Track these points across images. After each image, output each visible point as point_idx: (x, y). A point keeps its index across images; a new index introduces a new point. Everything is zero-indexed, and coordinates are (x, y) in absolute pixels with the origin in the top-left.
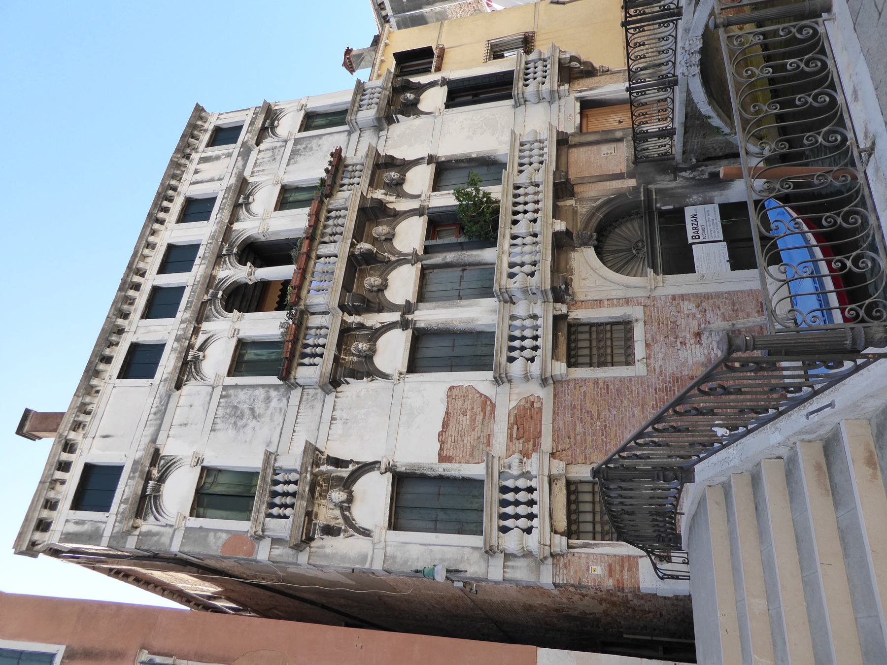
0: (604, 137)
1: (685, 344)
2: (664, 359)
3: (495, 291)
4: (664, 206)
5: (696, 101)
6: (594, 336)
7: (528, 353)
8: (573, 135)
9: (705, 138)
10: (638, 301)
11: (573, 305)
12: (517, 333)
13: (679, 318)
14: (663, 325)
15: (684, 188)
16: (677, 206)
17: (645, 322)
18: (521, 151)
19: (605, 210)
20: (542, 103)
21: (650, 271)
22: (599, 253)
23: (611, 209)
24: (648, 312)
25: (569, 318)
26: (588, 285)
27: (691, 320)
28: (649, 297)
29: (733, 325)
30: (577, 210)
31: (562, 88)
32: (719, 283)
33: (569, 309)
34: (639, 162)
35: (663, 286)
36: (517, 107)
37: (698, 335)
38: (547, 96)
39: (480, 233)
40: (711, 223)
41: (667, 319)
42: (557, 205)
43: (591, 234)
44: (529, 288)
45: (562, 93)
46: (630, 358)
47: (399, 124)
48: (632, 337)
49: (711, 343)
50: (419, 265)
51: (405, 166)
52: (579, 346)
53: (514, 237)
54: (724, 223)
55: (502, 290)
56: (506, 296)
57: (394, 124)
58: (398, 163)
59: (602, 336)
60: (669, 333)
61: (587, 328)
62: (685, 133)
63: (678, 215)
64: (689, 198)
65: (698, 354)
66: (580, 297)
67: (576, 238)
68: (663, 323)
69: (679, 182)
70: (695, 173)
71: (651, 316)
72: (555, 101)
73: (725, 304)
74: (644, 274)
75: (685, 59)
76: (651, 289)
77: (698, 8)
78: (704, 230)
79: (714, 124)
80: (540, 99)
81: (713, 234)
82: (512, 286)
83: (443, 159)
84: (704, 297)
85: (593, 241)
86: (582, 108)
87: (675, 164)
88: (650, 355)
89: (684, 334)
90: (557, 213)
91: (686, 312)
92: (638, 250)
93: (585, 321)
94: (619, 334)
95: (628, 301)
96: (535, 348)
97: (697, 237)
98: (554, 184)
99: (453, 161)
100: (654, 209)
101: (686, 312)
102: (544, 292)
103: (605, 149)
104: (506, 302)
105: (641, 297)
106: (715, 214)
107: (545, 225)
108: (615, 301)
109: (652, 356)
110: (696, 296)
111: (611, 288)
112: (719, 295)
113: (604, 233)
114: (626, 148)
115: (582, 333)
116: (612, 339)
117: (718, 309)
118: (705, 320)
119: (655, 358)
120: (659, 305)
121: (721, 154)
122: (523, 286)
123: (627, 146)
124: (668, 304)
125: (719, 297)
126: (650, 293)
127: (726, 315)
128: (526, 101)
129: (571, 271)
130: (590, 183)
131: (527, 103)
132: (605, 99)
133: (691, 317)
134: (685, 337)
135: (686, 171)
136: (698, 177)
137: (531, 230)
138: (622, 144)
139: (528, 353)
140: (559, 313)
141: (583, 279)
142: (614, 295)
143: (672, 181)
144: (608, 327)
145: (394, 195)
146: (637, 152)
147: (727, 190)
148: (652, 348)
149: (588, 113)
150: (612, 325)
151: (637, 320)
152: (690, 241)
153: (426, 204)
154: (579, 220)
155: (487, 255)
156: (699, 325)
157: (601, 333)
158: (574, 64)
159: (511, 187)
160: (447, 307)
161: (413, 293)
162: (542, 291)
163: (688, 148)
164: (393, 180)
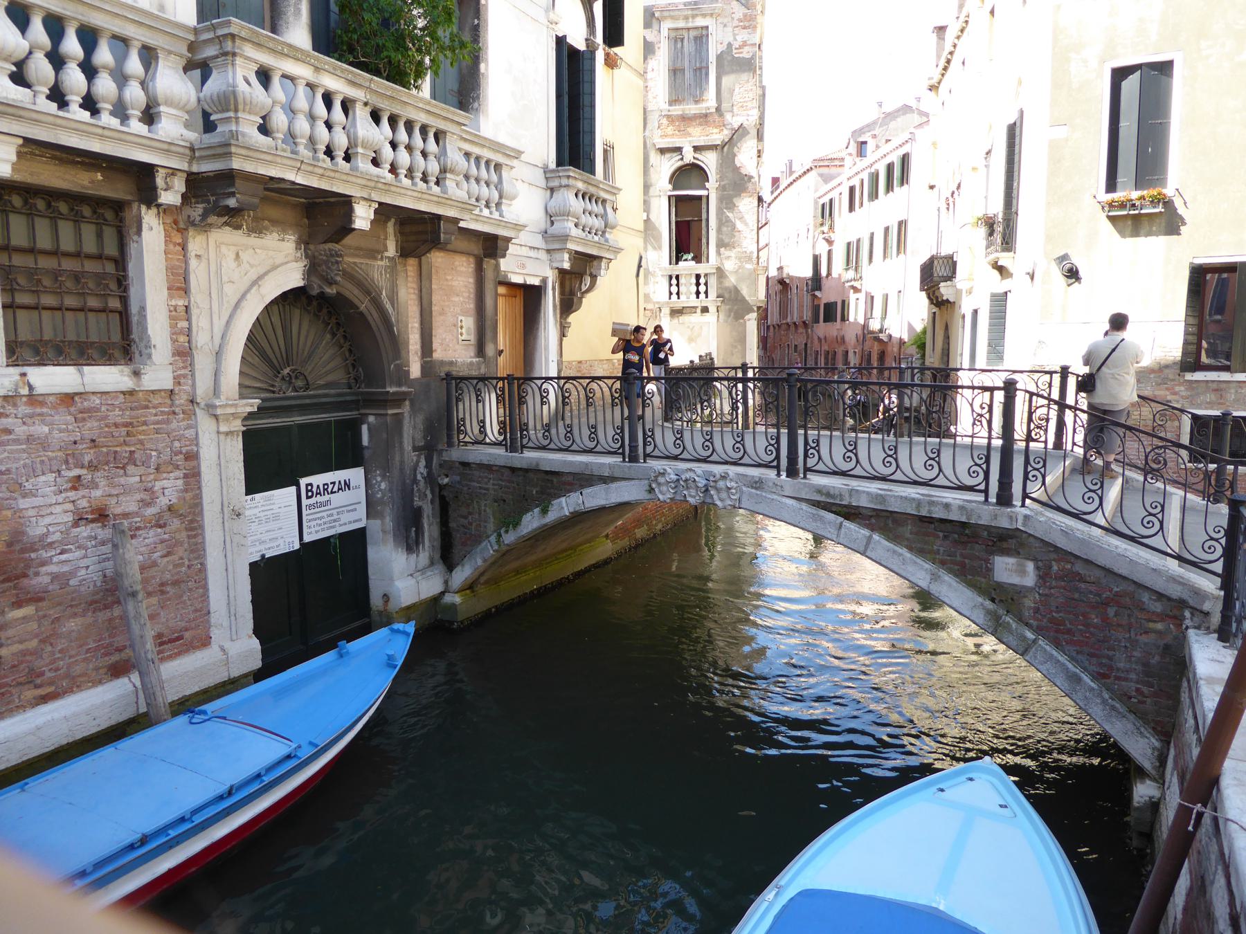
0: (488, 323)
1: (74, 488)
2: (30, 439)
3: (229, 22)
4: (369, 429)
5: (586, 491)
6: (90, 266)
7: (41, 68)
8: (497, 266)
9: (496, 501)
10: (185, 376)
11: (176, 222)
12: (104, 55)
13: (141, 470)
14: (124, 433)
15: (401, 465)
16: (367, 454)
17: (131, 393)
18: (488, 163)
19: (374, 317)
21: (252, 404)
22: (289, 299)
23: (375, 328)
24: (156, 400)
25: (143, 208)
26: (223, 264)
27: (138, 496)
28: (192, 401)
29: (134, 595)
30: (375, 258)
31: (566, 256)
32: (225, 548)
33: (165, 211)
34: (448, 384)
35: (218, 432)
37: (101, 515)
38: (558, 228)
39: (355, 31)
40: (335, 517)
41: (141, 442)
42: (389, 220)
43: (336, 283)
44: (231, 114)
45: (557, 256)
46: (27, 354)
48: (92, 362)
49: (79, 547)
52: (83, 226)
53: (347, 106)
54: (332, 540)
55: (230, 43)
56: (210, 51)
59: (91, 285)
60: (104, 450)
61: (111, 249)
62: (513, 470)
63: (349, 456)
64: (383, 476)
65: (48, 520)
66: (196, 243)
67: (330, 250)
68: (128, 434)
69: (410, 456)
70: (422, 483)
71: (147, 407)
72: (546, 242)
73: (176, 566)
74: (245, 391)
75: (697, 478)
76: (215, 407)
77: (804, 506)
78: (322, 504)
79: (527, 518)
80: (551, 217)
81: (315, 523)
82: (240, 73)
84: (192, 521)
85: (320, 287)
86: (533, 287)
87: (440, 447)
88: (42, 404)
89: (102, 483)
90: (384, 212)
91: (158, 485)
92: (288, 380)
93: (132, 248)
94: (98, 329)
95: (184, 354)
96: (58, 96)
97: (310, 494)
98: (438, 218)
99: (476, 22)
100: (363, 411)
101: (158, 485)
102: (224, 151)
103: (468, 323)
104: (192, 47)
105: (194, 386)
106: (350, 522)
107: (370, 184)
108: (185, 324)
109: (38, 410)
110: (196, 506)
111: (215, 317)
112: (198, 550)
113: (325, 311)
114: (469, 360)
115: (99, 235)
116: (81, 310)
117: (165, 552)
118: (138, 529)
119: (31, 416)
120: (174, 425)
121: (452, 525)
122: (240, 100)
123: (472, 363)
124: (177, 444)
125: (192, 551)
126: (202, 405)
127: (153, 572)
128: (552, 190)
129: (257, 229)
130: (421, 291)
131: (549, 192)
132: (538, 329)
133: (143, 495)
134: (94, 485)
135: (426, 467)
136: (416, 489)
137: (360, 150)
138: (472, 354)
139: (41, 68)
140: (160, 181)
141: (237, 255)
142: (200, 322)
144: (115, 303)
146: (475, 381)
147: (394, 541)
148: (62, 409)
149: (518, 298)
150: (120, 313)
151: (136, 374)
152: (304, 481)
155: (299, 33)
156: (126, 515)
157: (99, 284)
158: (588, 280)
159: (442, 125)
162: (230, 145)
163: (475, 472)
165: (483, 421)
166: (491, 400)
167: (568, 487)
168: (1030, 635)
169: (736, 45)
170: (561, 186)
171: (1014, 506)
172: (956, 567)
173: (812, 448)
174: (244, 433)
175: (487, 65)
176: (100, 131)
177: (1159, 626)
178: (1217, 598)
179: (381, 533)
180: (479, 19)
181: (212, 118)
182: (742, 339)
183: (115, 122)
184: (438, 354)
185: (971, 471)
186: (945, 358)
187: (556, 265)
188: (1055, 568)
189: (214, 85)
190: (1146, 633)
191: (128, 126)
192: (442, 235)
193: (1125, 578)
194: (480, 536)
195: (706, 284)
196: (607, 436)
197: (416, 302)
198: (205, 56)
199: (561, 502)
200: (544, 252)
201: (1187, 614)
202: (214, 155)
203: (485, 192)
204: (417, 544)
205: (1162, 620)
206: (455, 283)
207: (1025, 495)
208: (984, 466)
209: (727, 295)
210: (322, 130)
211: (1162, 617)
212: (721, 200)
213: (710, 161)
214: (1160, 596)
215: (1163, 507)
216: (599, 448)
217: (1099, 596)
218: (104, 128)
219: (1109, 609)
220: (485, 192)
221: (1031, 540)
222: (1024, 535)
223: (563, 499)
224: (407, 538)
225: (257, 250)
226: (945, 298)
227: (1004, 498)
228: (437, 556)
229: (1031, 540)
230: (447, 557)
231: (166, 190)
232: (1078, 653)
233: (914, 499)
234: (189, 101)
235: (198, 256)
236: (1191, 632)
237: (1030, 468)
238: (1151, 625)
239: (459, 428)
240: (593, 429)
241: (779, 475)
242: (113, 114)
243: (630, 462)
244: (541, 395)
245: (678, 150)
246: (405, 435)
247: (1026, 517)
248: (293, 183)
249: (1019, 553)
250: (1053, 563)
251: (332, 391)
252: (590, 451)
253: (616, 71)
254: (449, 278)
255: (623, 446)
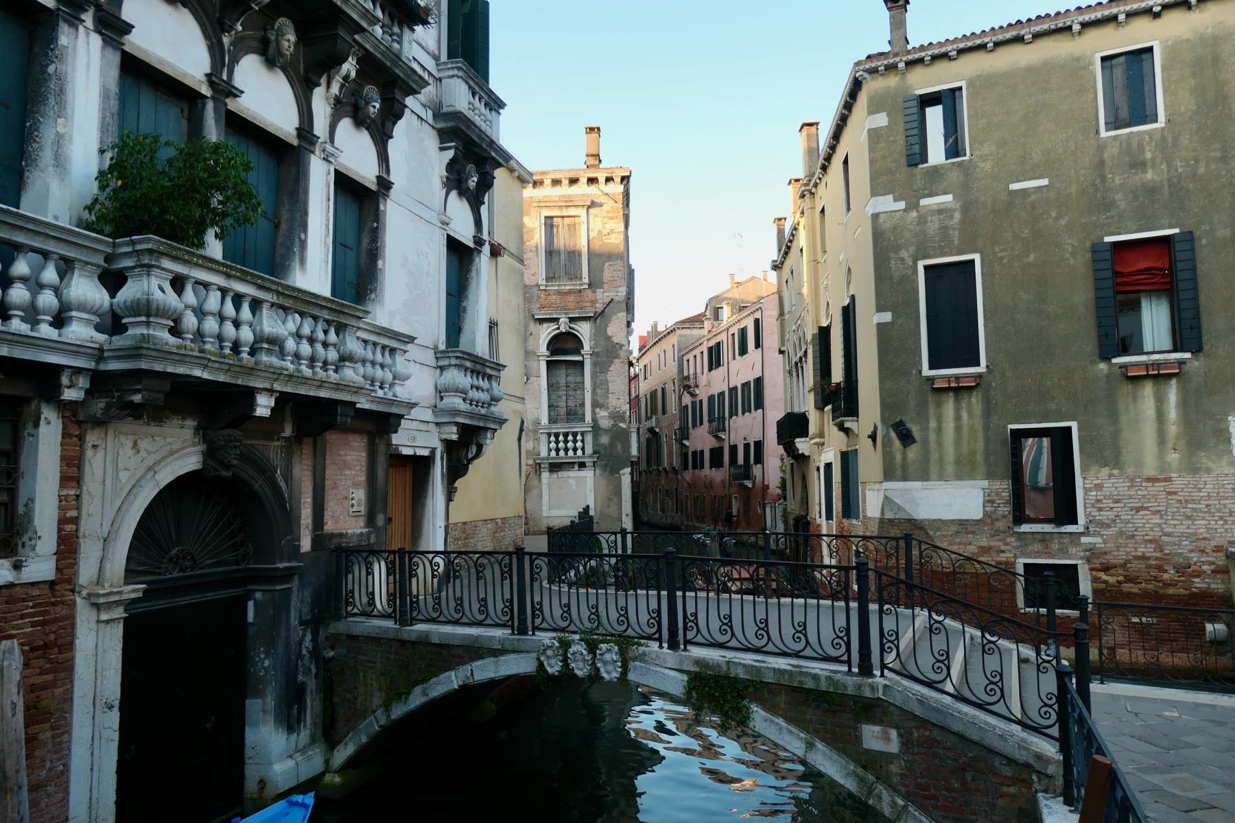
4: (255, 606)
8: (389, 444)
20: (433, 394)
21: (134, 591)
26: (121, 453)
30: (272, 440)
32: (92, 745)
36: (435, 353)
47: (437, 149)
50: (205, 90)
51: (381, 137)
57: (439, 141)
58: (388, 124)
64: (267, 654)
67: (229, 436)
72: (436, 416)
83: (382, 207)
99: (375, 225)
114: (359, 531)
123: (362, 534)
130: (315, 467)
131: (438, 370)
132: (426, 497)
135: (312, 640)
138: (362, 524)
140: (65, 380)
141: (135, 443)
143: (300, 617)
145: (340, 92)
147: (275, 721)
153: (317, 149)
154: (253, 442)
158: (474, 449)
160: (103, 118)
161: (145, 51)
164: (367, 103)
165: (373, 594)
166: (380, 569)
167: (458, 660)
168: (900, 802)
169: (605, 232)
170: (450, 365)
171: (874, 676)
172: (829, 736)
173: (690, 621)
174: (125, 619)
175: (384, 262)
176: (9, 337)
177: (1012, 790)
178: (1058, 761)
179: (261, 713)
180: (378, 223)
181: (124, 321)
182: (618, 492)
183: (24, 328)
184: (329, 527)
185: (835, 643)
186: (805, 507)
187: (444, 436)
188: (916, 735)
189: (128, 293)
190: (1001, 796)
191: (38, 331)
192: (339, 418)
193: (976, 744)
194: (366, 711)
195: (583, 441)
196: (497, 606)
197: (310, 478)
198: (121, 266)
199: (450, 676)
200: (433, 424)
201: (1034, 777)
202: (124, 356)
203: (379, 373)
204: (299, 722)
205: (1014, 784)
206: (348, 458)
207: (883, 667)
208: (845, 639)
209: (602, 452)
210: (229, 329)
211: (1014, 781)
212: (594, 365)
213: (584, 331)
214: (1010, 761)
215: (1001, 675)
216: (489, 621)
217: (956, 761)
218: (14, 334)
219: (966, 773)
220: (379, 373)
221: (892, 708)
222: (886, 704)
223: (453, 673)
224: (289, 716)
225: (156, 438)
226: (800, 452)
227: (866, 670)
228: (319, 733)
229: (892, 708)
230: (329, 736)
231: (69, 387)
232: (944, 819)
233: (785, 670)
234: (101, 306)
235: (95, 446)
236: (1040, 795)
237: (885, 641)
238: (1005, 789)
239: (347, 600)
240: (483, 602)
241: (661, 647)
242: (23, 319)
243: (518, 634)
244: (432, 569)
245: (556, 320)
246: (293, 611)
247: (885, 686)
248: (199, 378)
249: (882, 721)
250: (913, 730)
251: (220, 569)
252: (480, 624)
253: (499, 259)
254: (342, 453)
255: (512, 618)
